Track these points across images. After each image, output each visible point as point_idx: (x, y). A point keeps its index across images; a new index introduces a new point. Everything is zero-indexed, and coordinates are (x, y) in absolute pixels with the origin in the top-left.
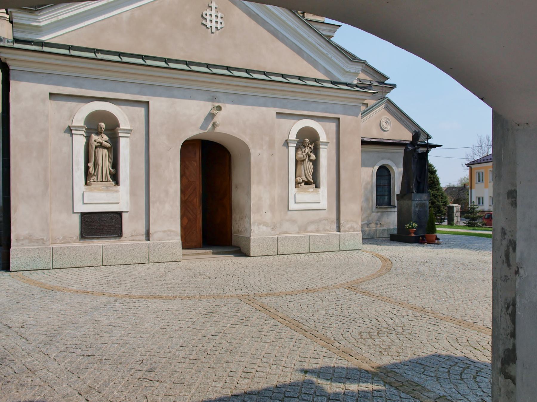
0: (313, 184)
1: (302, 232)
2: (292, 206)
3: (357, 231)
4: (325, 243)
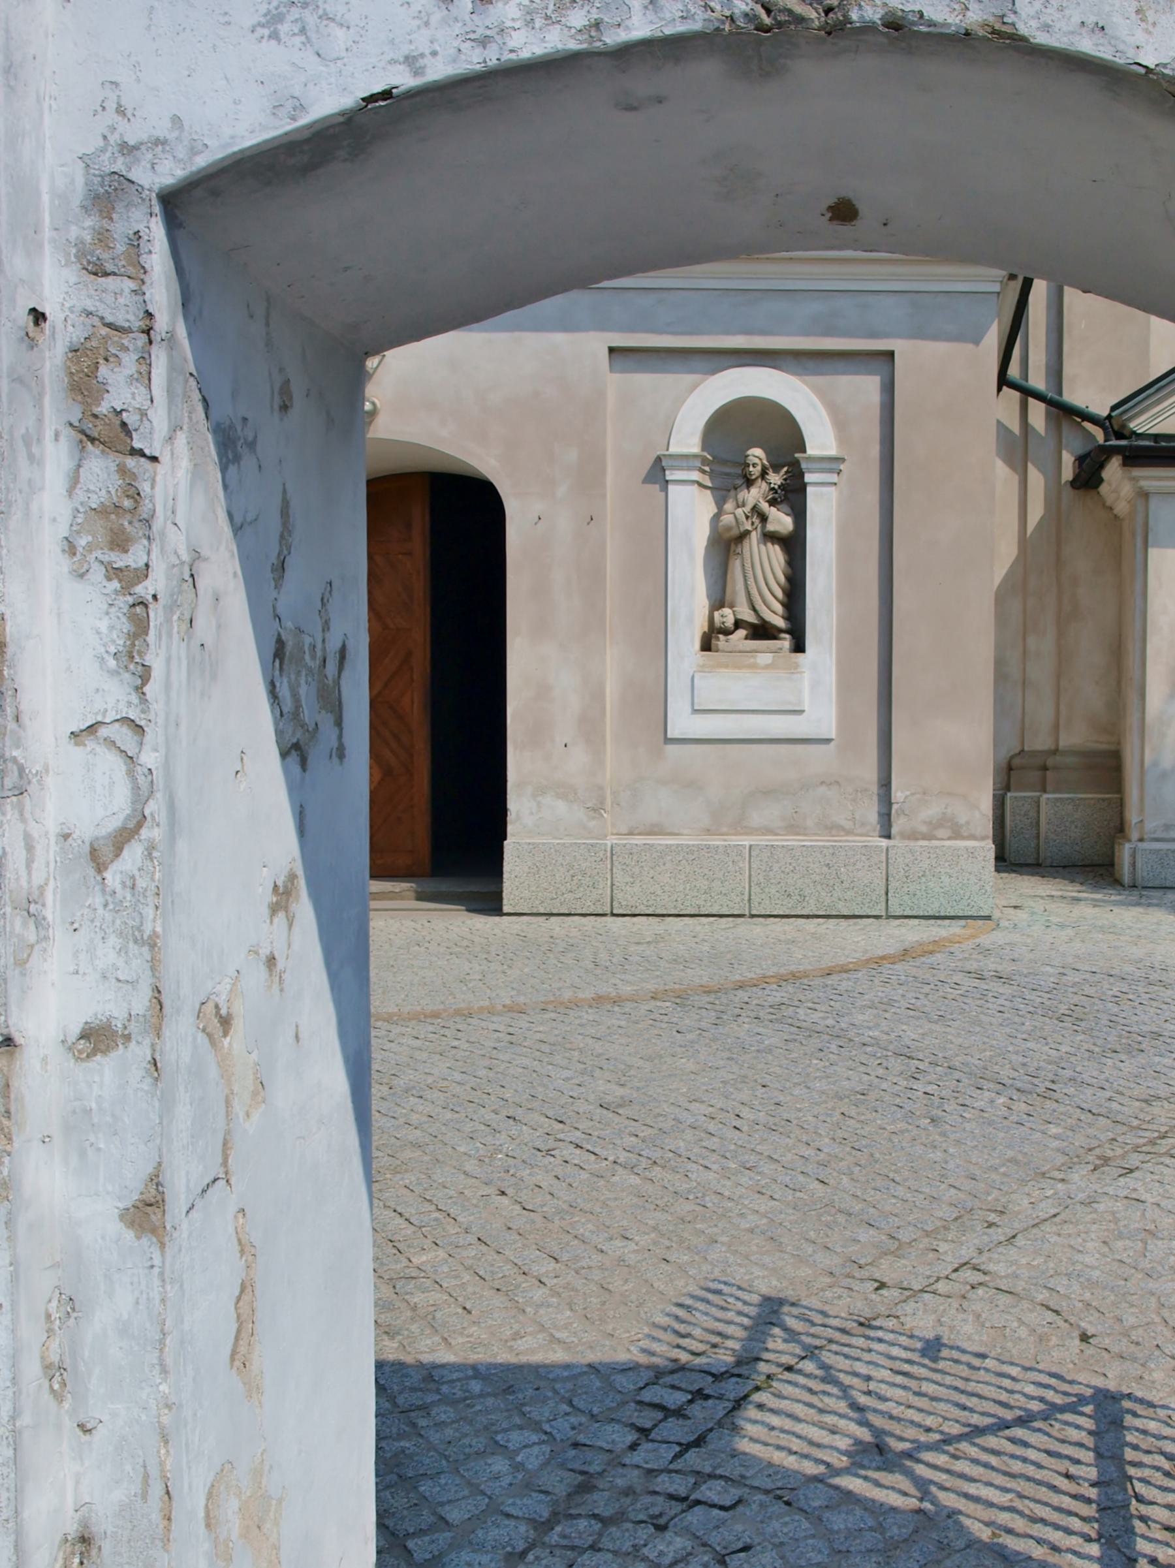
0: (783, 635)
1: (725, 830)
2: (682, 723)
3: (972, 837)
4: (818, 878)
